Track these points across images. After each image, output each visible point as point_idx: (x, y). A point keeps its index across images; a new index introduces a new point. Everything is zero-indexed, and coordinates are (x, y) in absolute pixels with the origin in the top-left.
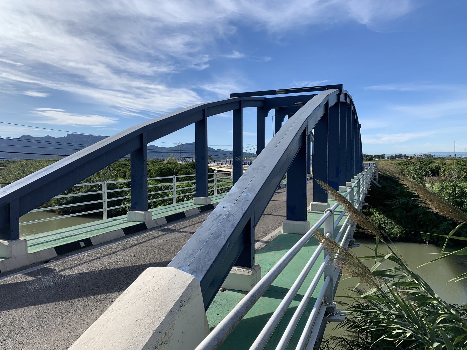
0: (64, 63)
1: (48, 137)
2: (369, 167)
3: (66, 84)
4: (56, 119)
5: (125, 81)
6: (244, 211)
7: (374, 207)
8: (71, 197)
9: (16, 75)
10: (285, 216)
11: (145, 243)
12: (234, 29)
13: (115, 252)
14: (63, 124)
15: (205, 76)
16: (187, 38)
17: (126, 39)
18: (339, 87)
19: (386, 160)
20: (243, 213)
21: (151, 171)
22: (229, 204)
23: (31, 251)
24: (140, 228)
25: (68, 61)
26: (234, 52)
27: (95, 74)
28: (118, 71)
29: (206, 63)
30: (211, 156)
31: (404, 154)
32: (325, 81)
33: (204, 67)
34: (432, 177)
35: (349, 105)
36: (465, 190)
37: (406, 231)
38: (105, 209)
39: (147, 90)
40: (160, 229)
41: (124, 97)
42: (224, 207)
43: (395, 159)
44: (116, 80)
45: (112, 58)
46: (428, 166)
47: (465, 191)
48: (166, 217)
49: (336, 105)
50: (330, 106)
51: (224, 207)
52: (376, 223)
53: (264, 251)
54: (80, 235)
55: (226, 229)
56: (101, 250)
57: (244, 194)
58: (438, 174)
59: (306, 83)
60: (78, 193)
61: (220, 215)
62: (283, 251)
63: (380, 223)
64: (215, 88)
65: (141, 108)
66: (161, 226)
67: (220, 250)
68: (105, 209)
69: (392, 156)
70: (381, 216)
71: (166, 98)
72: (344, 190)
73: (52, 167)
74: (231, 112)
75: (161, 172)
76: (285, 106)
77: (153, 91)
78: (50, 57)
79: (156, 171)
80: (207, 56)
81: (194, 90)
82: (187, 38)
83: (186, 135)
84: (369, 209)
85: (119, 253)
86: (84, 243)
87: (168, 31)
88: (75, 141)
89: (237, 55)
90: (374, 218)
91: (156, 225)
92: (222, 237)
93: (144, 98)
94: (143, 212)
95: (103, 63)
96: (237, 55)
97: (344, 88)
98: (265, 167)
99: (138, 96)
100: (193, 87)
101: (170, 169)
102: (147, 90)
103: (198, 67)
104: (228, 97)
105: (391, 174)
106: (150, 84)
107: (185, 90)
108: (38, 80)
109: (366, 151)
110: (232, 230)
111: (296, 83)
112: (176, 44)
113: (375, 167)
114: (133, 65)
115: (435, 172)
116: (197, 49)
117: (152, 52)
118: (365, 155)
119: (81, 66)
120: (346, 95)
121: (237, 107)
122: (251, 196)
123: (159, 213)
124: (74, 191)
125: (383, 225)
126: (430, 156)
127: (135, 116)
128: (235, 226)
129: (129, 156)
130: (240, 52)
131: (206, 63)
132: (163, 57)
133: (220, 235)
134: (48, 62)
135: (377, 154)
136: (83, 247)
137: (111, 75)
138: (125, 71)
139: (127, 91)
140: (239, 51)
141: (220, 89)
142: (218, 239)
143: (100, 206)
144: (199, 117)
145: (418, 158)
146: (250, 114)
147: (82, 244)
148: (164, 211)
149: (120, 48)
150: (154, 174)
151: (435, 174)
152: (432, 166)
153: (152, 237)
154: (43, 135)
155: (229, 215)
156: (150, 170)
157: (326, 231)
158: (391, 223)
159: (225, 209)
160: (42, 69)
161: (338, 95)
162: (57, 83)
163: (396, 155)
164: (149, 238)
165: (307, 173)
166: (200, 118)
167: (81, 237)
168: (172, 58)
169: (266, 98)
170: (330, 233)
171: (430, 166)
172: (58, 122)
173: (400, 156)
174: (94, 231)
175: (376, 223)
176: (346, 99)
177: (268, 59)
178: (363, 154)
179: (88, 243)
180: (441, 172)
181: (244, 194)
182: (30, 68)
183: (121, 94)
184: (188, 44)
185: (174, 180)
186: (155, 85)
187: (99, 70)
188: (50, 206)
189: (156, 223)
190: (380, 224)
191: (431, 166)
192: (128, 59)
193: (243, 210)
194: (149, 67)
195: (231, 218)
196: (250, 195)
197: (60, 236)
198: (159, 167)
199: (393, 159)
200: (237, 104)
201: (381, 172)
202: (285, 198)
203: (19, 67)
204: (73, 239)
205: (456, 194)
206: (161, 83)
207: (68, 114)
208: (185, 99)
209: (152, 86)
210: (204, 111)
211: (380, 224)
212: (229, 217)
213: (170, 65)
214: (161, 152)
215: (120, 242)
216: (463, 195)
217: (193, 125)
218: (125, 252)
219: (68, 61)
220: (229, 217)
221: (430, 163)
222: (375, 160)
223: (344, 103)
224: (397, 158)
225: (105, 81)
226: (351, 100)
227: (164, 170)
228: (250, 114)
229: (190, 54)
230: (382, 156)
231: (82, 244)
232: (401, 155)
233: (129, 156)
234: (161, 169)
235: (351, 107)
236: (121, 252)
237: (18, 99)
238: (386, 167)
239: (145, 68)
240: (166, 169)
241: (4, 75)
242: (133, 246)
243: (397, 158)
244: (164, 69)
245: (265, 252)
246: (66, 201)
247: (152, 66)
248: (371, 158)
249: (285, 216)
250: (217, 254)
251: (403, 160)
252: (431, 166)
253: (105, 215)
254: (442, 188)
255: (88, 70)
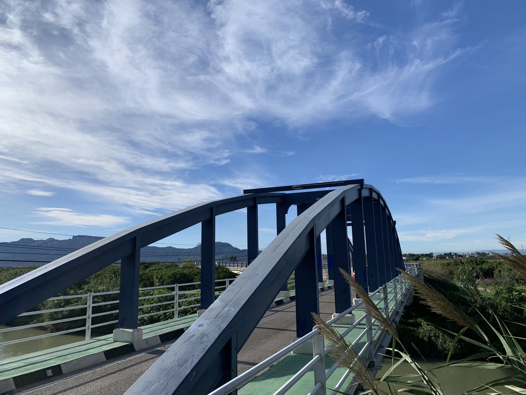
0: (74, 160)
1: (51, 240)
2: (412, 268)
3: (74, 183)
4: (60, 220)
5: (138, 177)
6: (221, 330)
7: (421, 317)
8: (67, 311)
9: (20, 174)
10: (294, 331)
11: (128, 369)
12: (253, 126)
13: (87, 382)
14: (69, 225)
15: (224, 171)
16: (205, 134)
17: (141, 135)
18: (360, 182)
19: (434, 260)
20: (219, 333)
21: (164, 277)
22: (207, 321)
23: (144, 337)
24: (128, 350)
25: (78, 158)
26: (255, 147)
27: (106, 170)
28: (131, 168)
29: (226, 158)
30: (236, 257)
31: (455, 252)
32: (353, 175)
33: (224, 162)
34: (486, 280)
35: (375, 200)
36: (523, 294)
37: (461, 345)
38: (89, 326)
39: (163, 187)
40: (150, 351)
41: (138, 195)
42: (200, 326)
43: (445, 258)
44: (130, 177)
45: (126, 154)
46: (479, 266)
47: (524, 295)
48: (159, 335)
49: (357, 202)
50: (348, 202)
51: (200, 326)
52: (425, 335)
53: (264, 378)
54: (49, 362)
55: (195, 354)
56: (70, 381)
57: (226, 309)
58: (492, 276)
59: (333, 177)
60: (77, 305)
61: (193, 336)
62: (286, 377)
63: (429, 336)
64: (236, 183)
65: (157, 205)
66: (153, 347)
67: (182, 380)
68: (89, 326)
69: (441, 255)
70: (429, 328)
71: (184, 195)
72: (376, 297)
73: (22, 279)
74: (246, 208)
75: (175, 278)
76: (304, 202)
77: (169, 187)
78: (60, 154)
79: (169, 277)
80: (228, 151)
81: (214, 185)
82: (205, 134)
83: (189, 239)
84: (416, 318)
85: (91, 384)
86: (53, 372)
87: (185, 127)
88: (29, 251)
89: (258, 150)
90: (422, 330)
91: (146, 346)
92: (189, 363)
93: (160, 195)
94: (131, 331)
95: (115, 159)
96: (258, 150)
97: (366, 183)
98: (258, 274)
99: (153, 193)
100: (213, 182)
101: (186, 275)
102: (163, 187)
103: (218, 163)
104: (242, 194)
105: (438, 277)
106: (167, 180)
107: (201, 186)
108: (39, 178)
109: (405, 249)
110: (202, 355)
111: (323, 178)
112: (194, 140)
113: (418, 269)
114: (148, 162)
115: (488, 274)
116: (215, 145)
117: (168, 148)
118: (405, 255)
119: (92, 162)
120: (371, 190)
121: (251, 204)
122: (234, 311)
123: (150, 332)
124: (71, 303)
125: (433, 338)
126: (484, 254)
127: (149, 215)
128: (207, 349)
129: (120, 261)
130: (262, 147)
131: (226, 158)
132: (179, 152)
133: (186, 361)
134: (56, 159)
135: (425, 253)
136: (50, 377)
137: (124, 172)
138: (139, 168)
139: (141, 188)
140: (260, 146)
141: (242, 184)
142: (184, 367)
143: (94, 321)
144: (205, 216)
145: (470, 256)
146: (267, 212)
147: (50, 373)
148: (160, 327)
149: (134, 145)
150: (166, 281)
151: (489, 276)
152: (485, 266)
153: (137, 361)
154: (45, 238)
155: (203, 335)
156: (162, 276)
157: (316, 353)
158: (443, 336)
159: (200, 328)
160: (50, 167)
161: (360, 191)
162: (63, 180)
163: (445, 254)
164: (134, 363)
165: (317, 280)
166: (207, 217)
167: (51, 363)
168: (191, 153)
169: (285, 194)
170: (320, 355)
171: (483, 266)
172: (62, 223)
173: (450, 255)
174: (68, 356)
175: (425, 335)
176: (371, 194)
177: (291, 153)
178: (404, 251)
179: (57, 372)
180: (496, 272)
181: (226, 309)
182: (37, 166)
183: (133, 192)
184: (206, 140)
185: (177, 289)
186: (172, 181)
187: (112, 167)
188: (42, 322)
189: (147, 343)
190: (430, 337)
191: (484, 266)
192: (142, 155)
193: (220, 329)
194: (166, 163)
195: (205, 339)
196: (233, 309)
197: (24, 363)
198: (172, 272)
199: (442, 258)
200: (251, 200)
201: (427, 274)
202: (294, 309)
203: (25, 165)
204: (39, 367)
205: (513, 300)
206: (177, 179)
207: (74, 213)
208: (203, 195)
209: (168, 183)
210: (212, 209)
211: (430, 337)
212: (202, 337)
213: (188, 161)
214: (179, 255)
215: (98, 370)
216: (522, 300)
217: (199, 225)
218: (99, 383)
219: (78, 158)
220: (202, 337)
221: (483, 262)
222: (422, 260)
223: (369, 199)
224: (447, 258)
225: (116, 178)
226: (379, 195)
227: (178, 276)
228: (267, 212)
229: (209, 150)
230: (430, 256)
231: (50, 373)
232: (451, 253)
233: (120, 261)
234: (175, 275)
235: (379, 202)
236: (93, 383)
237: (22, 197)
238: (432, 268)
239: (162, 164)
240: (181, 275)
241: (7, 173)
242: (111, 374)
243: (447, 258)
244: (181, 165)
245: (264, 379)
246: (61, 316)
247: (169, 162)
248: (416, 258)
249: (294, 331)
250: (177, 386)
251: (451, 260)
252: (484, 266)
253: (88, 333)
254: (497, 292)
255: (99, 167)
